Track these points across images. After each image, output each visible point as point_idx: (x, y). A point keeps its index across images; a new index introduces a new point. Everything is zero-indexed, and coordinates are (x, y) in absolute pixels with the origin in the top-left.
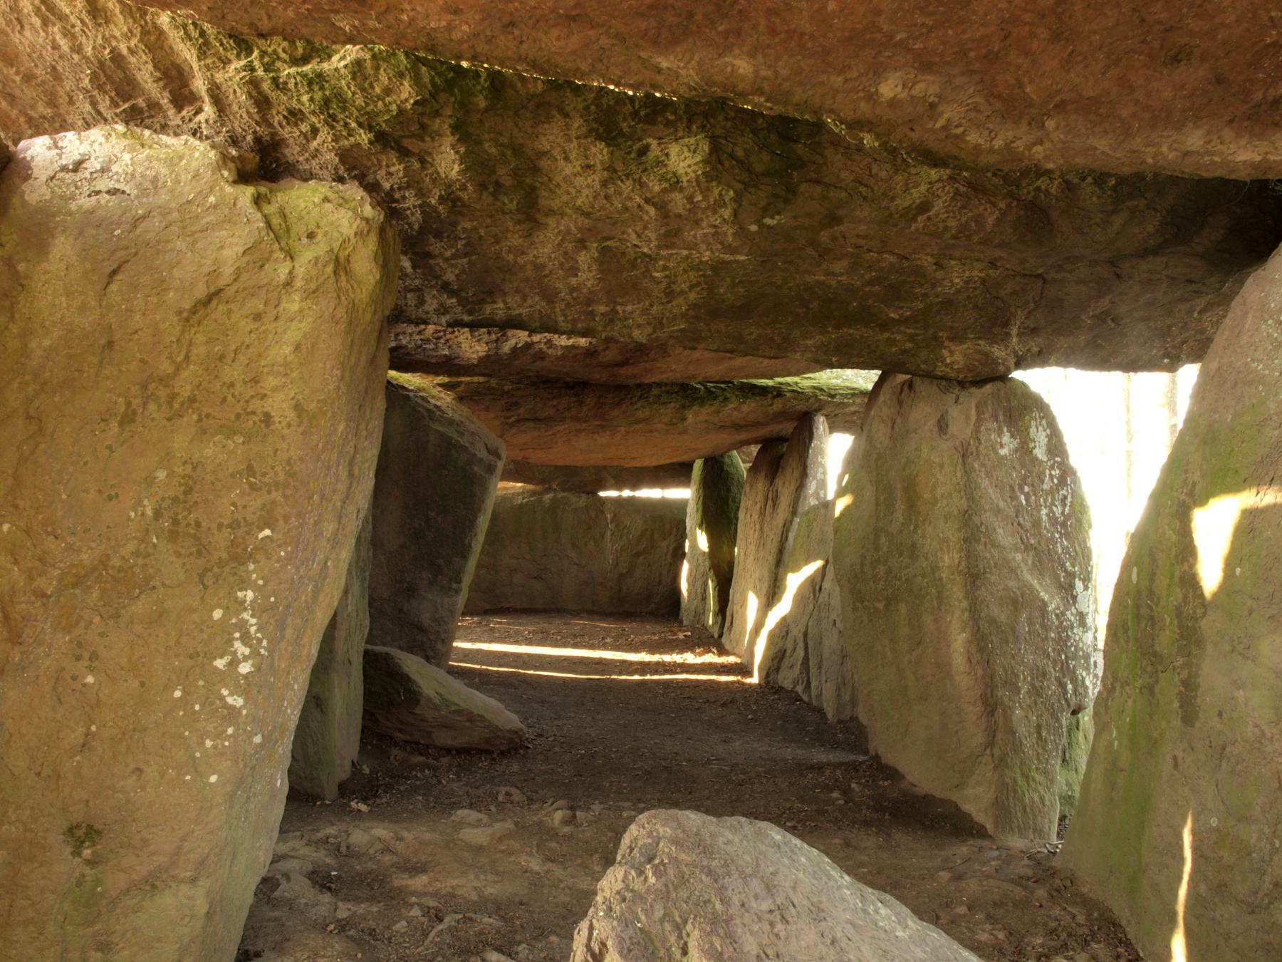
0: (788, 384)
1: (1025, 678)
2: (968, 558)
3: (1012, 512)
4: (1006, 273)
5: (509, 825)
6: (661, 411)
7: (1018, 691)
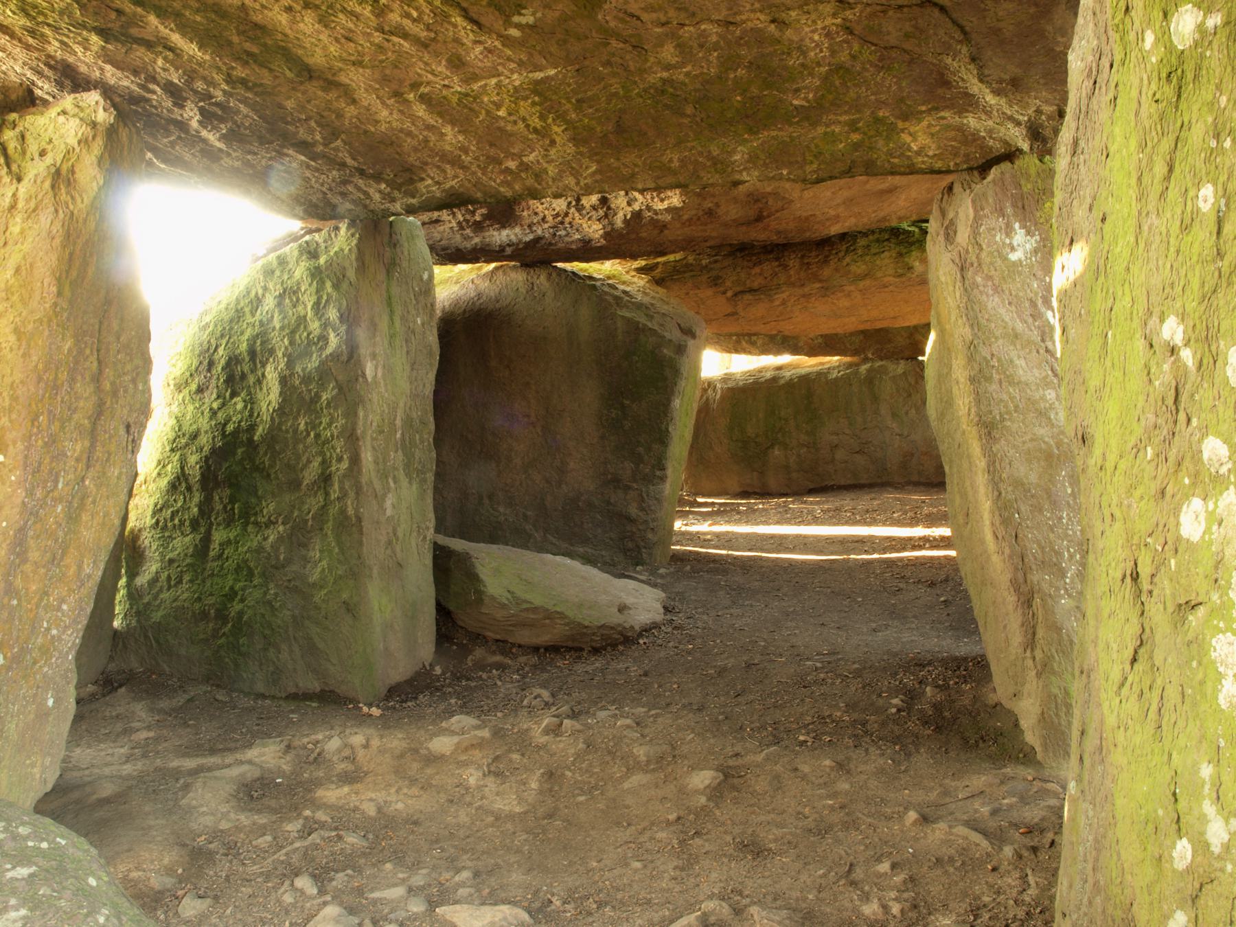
1: (1071, 556)
2: (978, 401)
3: (1035, 336)
4: (868, 9)
5: (486, 733)
6: (878, 262)
7: (1062, 573)
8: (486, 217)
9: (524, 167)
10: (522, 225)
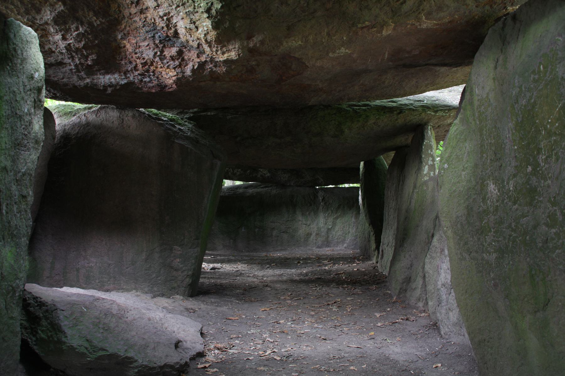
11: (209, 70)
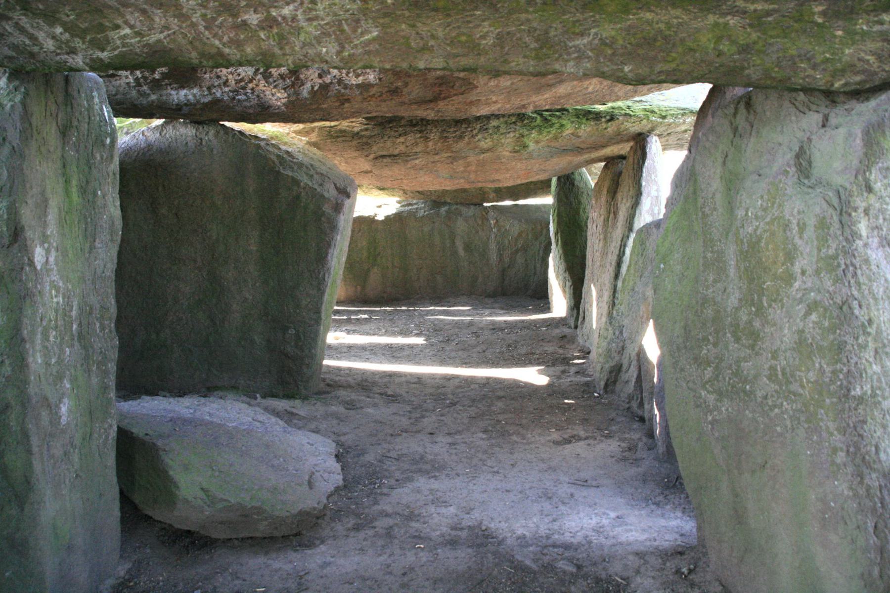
0: (620, 108)
6: (503, 141)
8: (165, 76)
9: (270, 23)
10: (201, 87)
11: (335, 91)
